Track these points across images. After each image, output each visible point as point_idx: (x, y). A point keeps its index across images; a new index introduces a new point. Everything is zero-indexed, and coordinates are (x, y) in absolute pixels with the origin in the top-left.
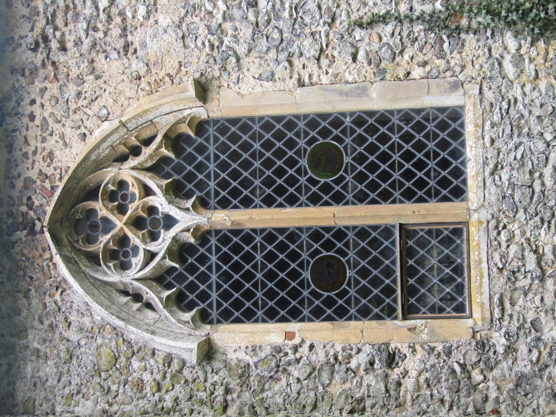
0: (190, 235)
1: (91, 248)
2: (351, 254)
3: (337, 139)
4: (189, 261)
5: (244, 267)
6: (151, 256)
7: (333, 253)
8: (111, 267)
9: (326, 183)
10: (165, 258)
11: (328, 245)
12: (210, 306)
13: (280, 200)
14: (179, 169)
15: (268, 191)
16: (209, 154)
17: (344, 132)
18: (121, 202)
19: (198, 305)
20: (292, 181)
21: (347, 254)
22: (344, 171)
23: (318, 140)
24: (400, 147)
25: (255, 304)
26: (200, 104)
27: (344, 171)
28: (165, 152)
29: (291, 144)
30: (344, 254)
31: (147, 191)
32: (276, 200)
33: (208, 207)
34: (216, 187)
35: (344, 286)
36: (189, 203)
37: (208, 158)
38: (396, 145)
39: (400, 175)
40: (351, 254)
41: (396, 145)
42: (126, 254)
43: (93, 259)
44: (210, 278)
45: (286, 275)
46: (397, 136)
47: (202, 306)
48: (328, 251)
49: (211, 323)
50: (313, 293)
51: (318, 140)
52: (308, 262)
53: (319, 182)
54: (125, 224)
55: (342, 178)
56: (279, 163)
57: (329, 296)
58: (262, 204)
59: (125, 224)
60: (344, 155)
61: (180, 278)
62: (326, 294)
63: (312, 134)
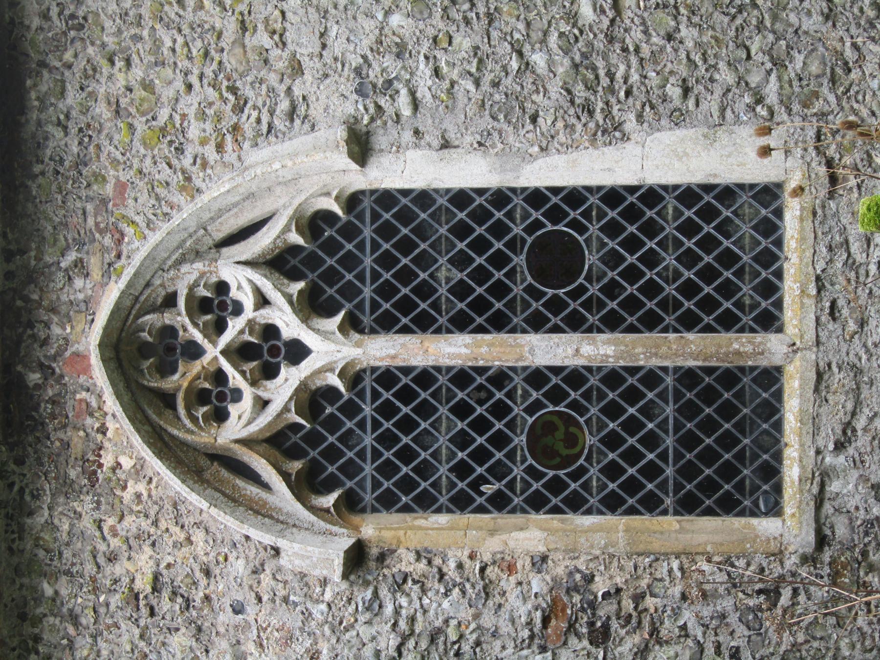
0: (333, 201)
1: (169, 383)
2: (594, 229)
3: (575, 225)
4: (328, 411)
5: (418, 306)
7: (565, 407)
8: (198, 418)
9: (556, 405)
10: (290, 230)
11: (555, 214)
12: (361, 484)
13: (479, 320)
14: (313, 439)
15: (461, 215)
16: (364, 270)
17: (587, 396)
18: (216, 302)
19: (342, 484)
20: (500, 290)
21: (587, 229)
22: (585, 279)
23: (543, 226)
24: (678, 305)
25: (435, 306)
26: (354, 166)
27: (585, 279)
28: (295, 238)
29: (499, 230)
30: (581, 229)
31: (263, 301)
32: (473, 320)
33: (361, 506)
34: (374, 473)
35: (581, 280)
36: (329, 500)
37: (361, 277)
38: (671, 302)
39: (677, 229)
40: (594, 229)
41: (671, 302)
42: (221, 397)
43: (168, 400)
44: (362, 470)
45: (487, 440)
46: (672, 317)
47: (349, 484)
48: (555, 223)
49: (361, 332)
50: (530, 470)
51: (544, 226)
52: (524, 241)
53: (545, 474)
54: (223, 352)
55: (582, 290)
56: (479, 260)
57: (555, 296)
58: (451, 506)
59: (223, 352)
60: (587, 252)
61: (313, 261)
62: (550, 292)
63: (535, 215)
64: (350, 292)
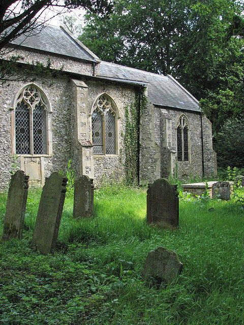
6: (27, 100)
64: (19, 109)
